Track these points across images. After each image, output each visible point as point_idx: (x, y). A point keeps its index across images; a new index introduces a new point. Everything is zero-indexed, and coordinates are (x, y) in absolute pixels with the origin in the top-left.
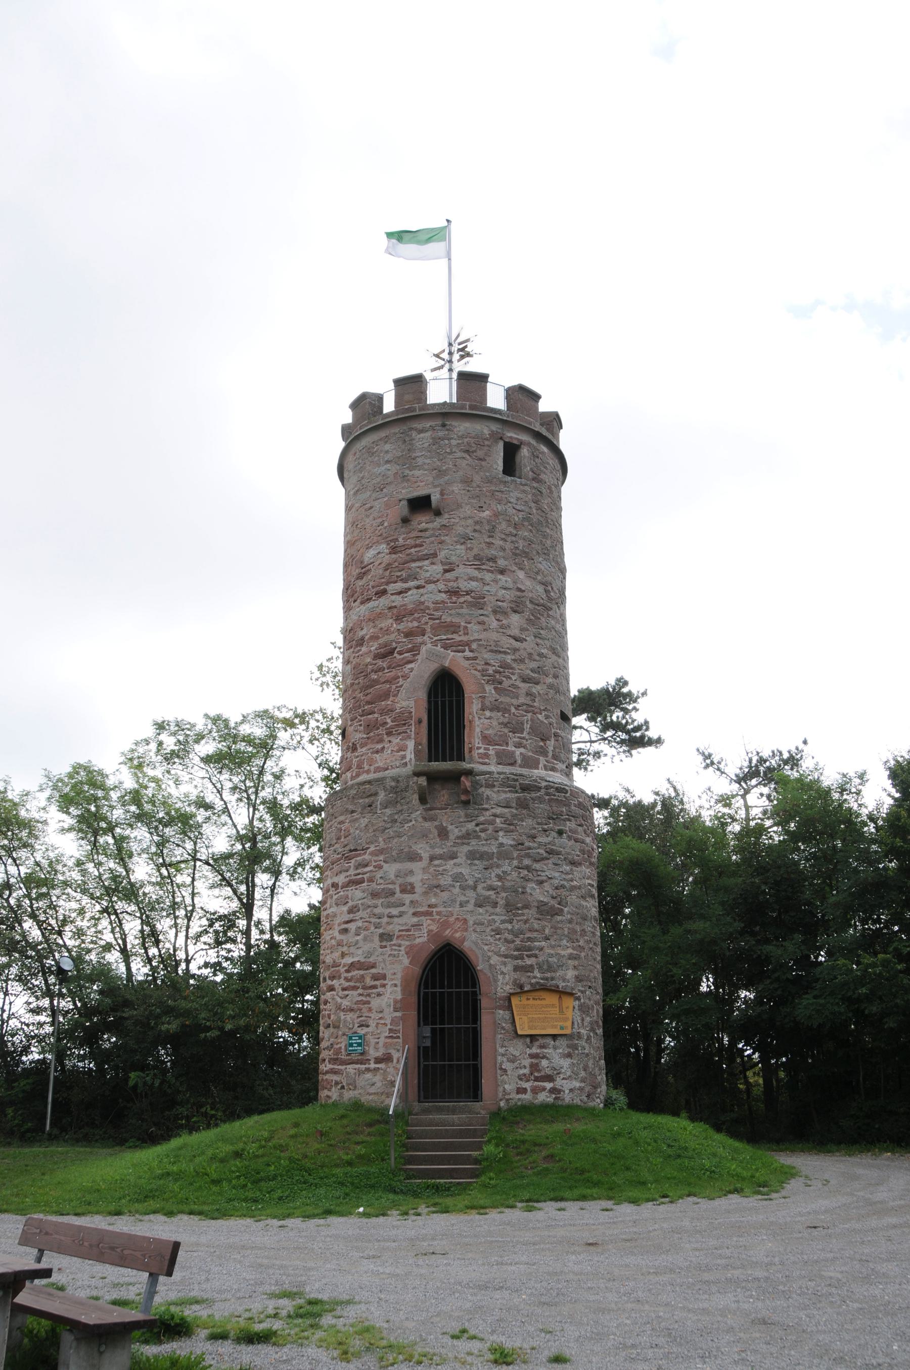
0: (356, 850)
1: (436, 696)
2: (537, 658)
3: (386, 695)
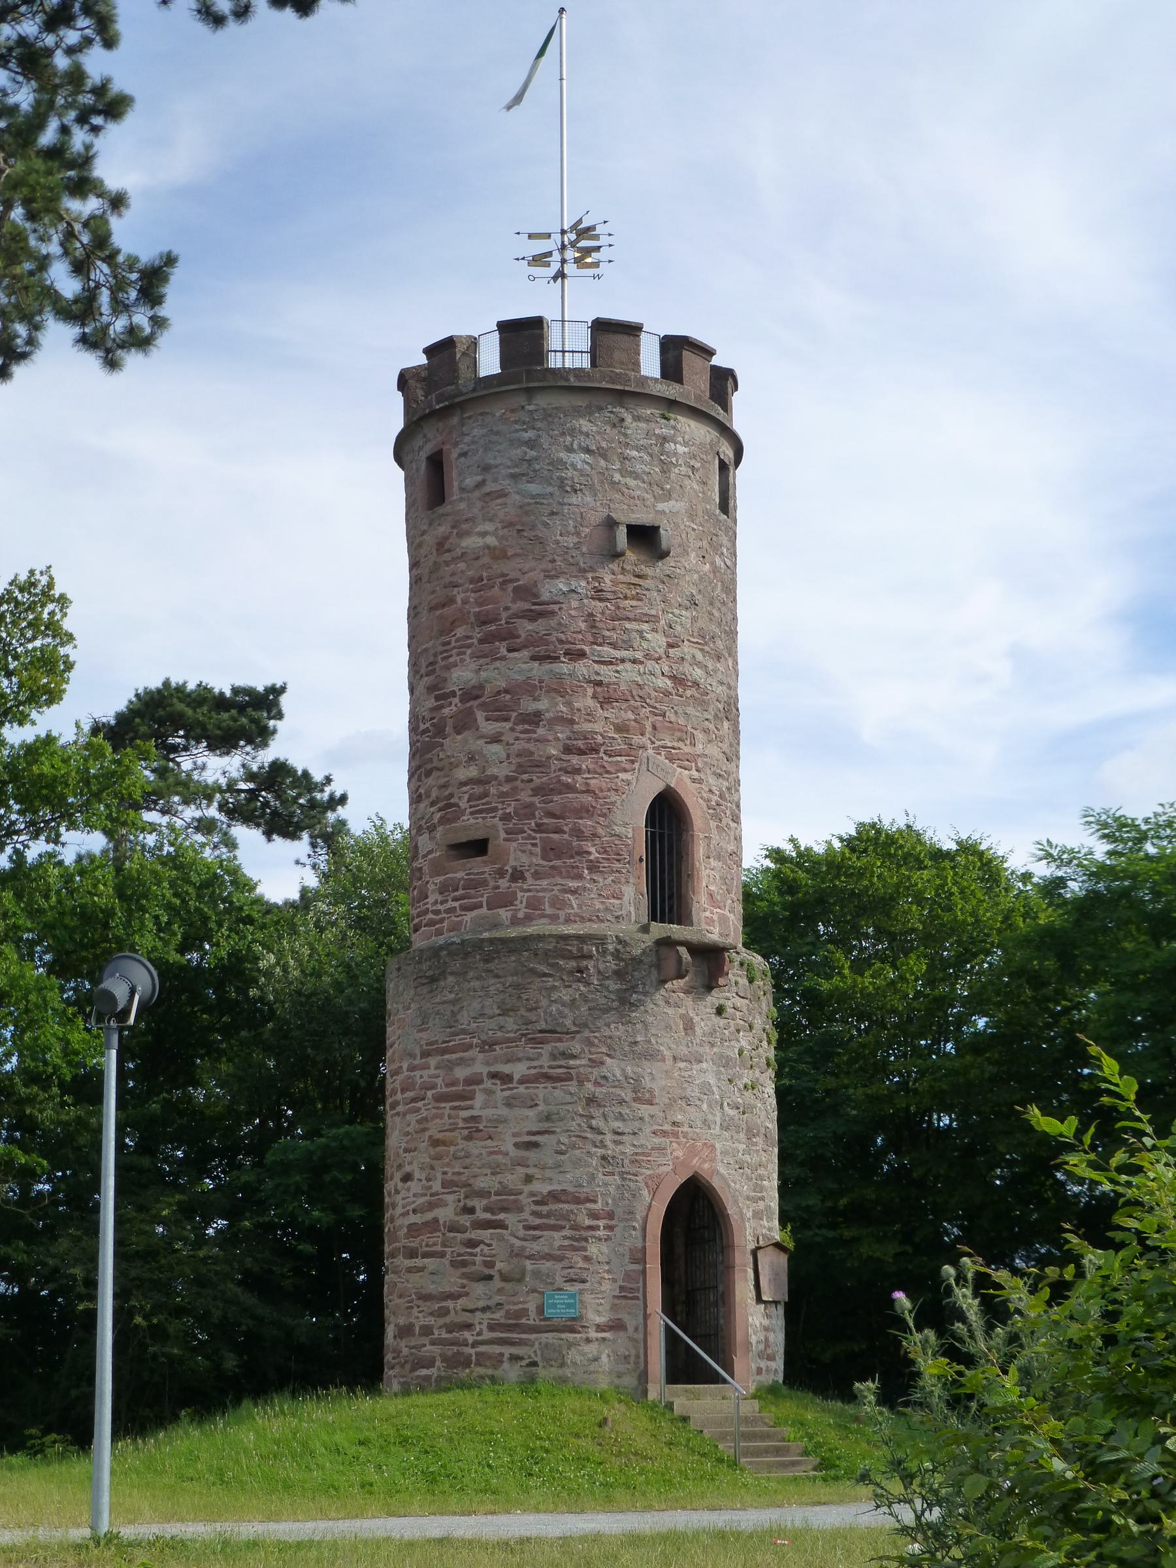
3: (585, 811)
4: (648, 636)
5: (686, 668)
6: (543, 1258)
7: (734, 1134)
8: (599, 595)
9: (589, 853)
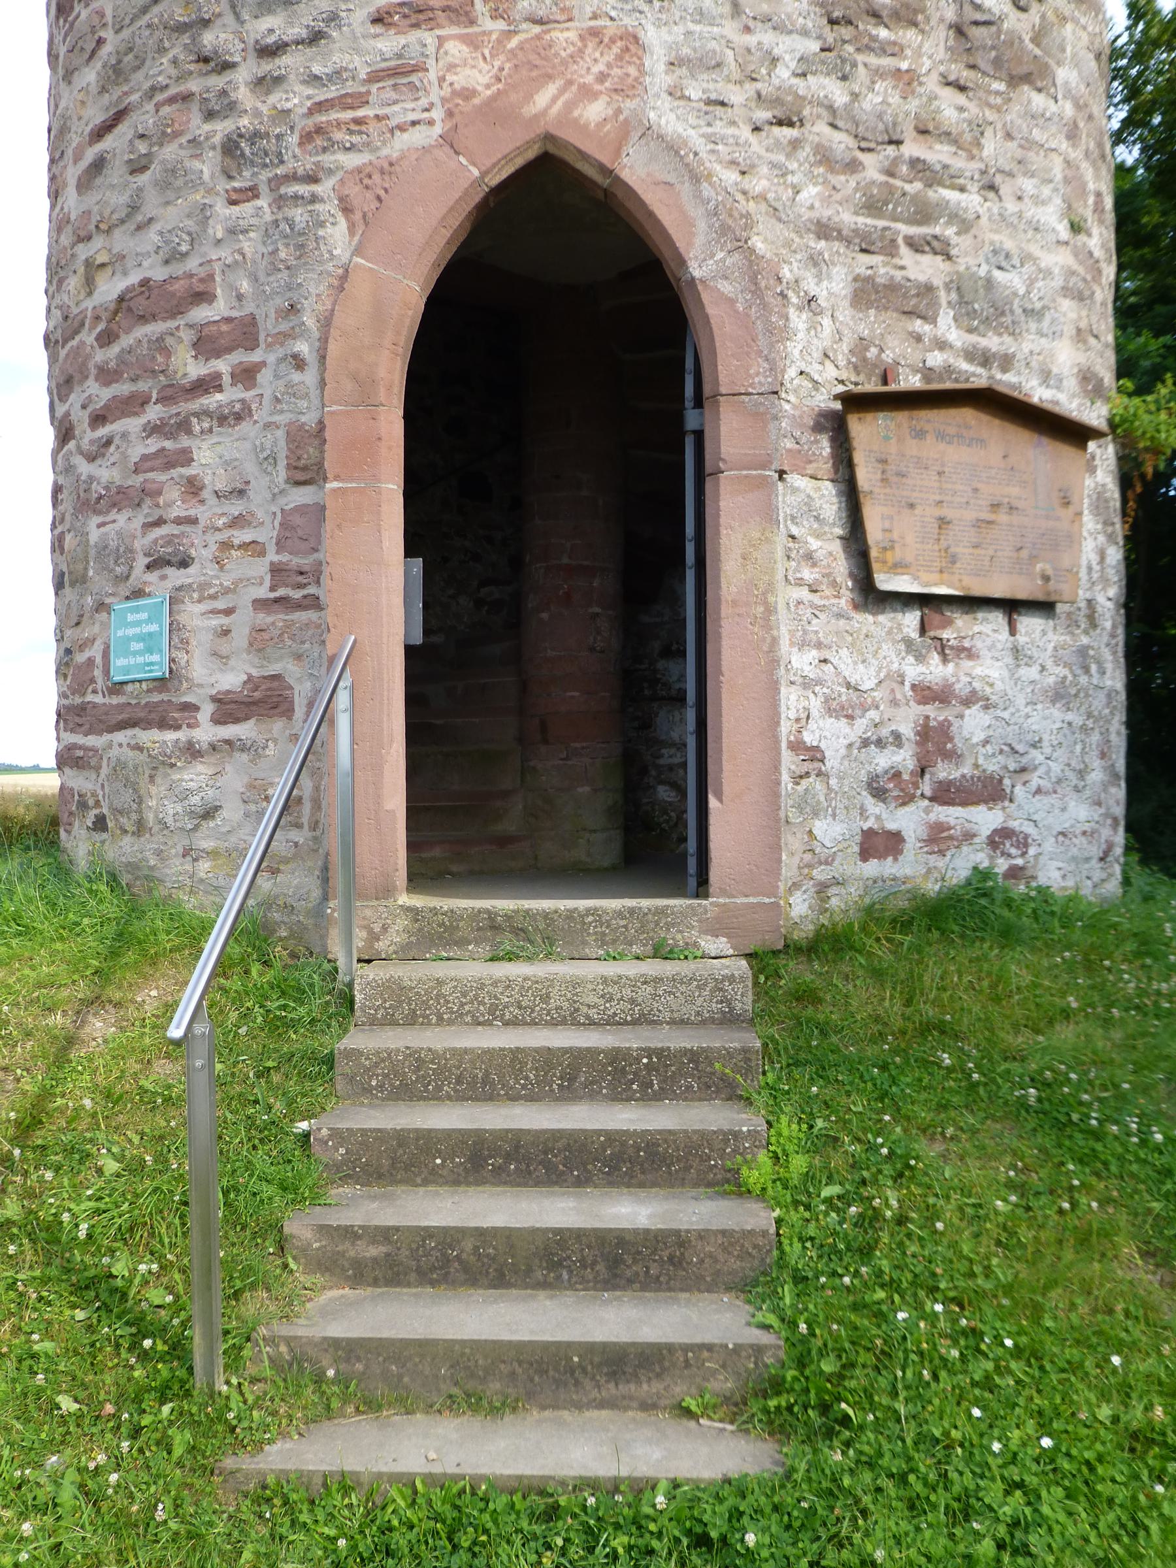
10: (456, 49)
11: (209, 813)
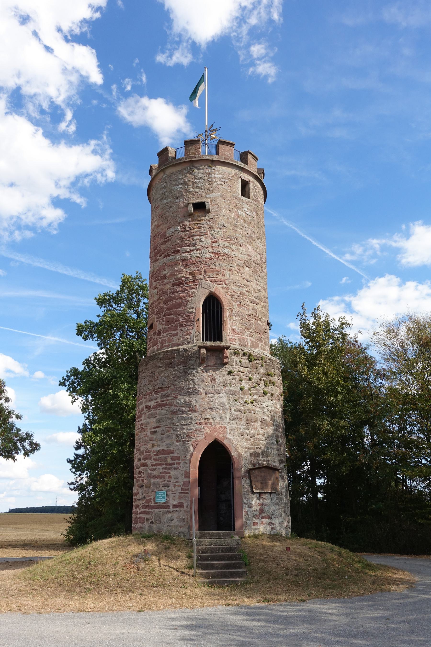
0: (161, 388)
1: (206, 307)
2: (257, 291)
3: (179, 305)
4: (203, 240)
5: (220, 249)
6: (156, 477)
7: (238, 422)
8: (184, 230)
9: (180, 320)
10: (206, 428)
11: (172, 520)
